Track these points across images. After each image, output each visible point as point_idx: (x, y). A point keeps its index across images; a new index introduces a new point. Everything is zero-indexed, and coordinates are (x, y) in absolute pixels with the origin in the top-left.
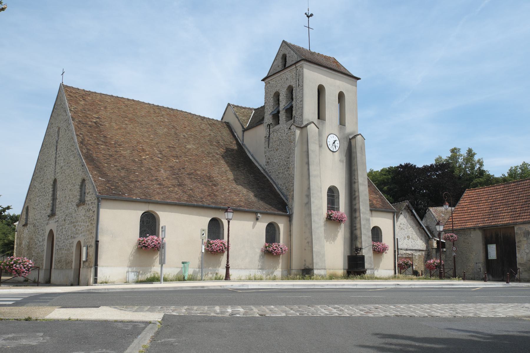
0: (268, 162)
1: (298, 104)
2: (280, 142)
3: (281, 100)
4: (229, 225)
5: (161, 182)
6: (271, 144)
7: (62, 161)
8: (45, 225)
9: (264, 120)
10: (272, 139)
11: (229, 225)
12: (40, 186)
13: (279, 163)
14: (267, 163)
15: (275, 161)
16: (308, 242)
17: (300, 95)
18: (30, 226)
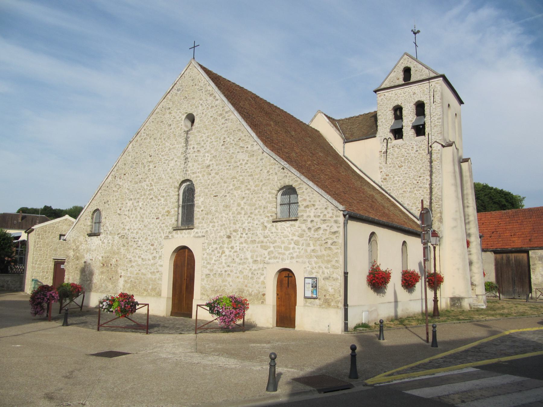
15: (398, 179)
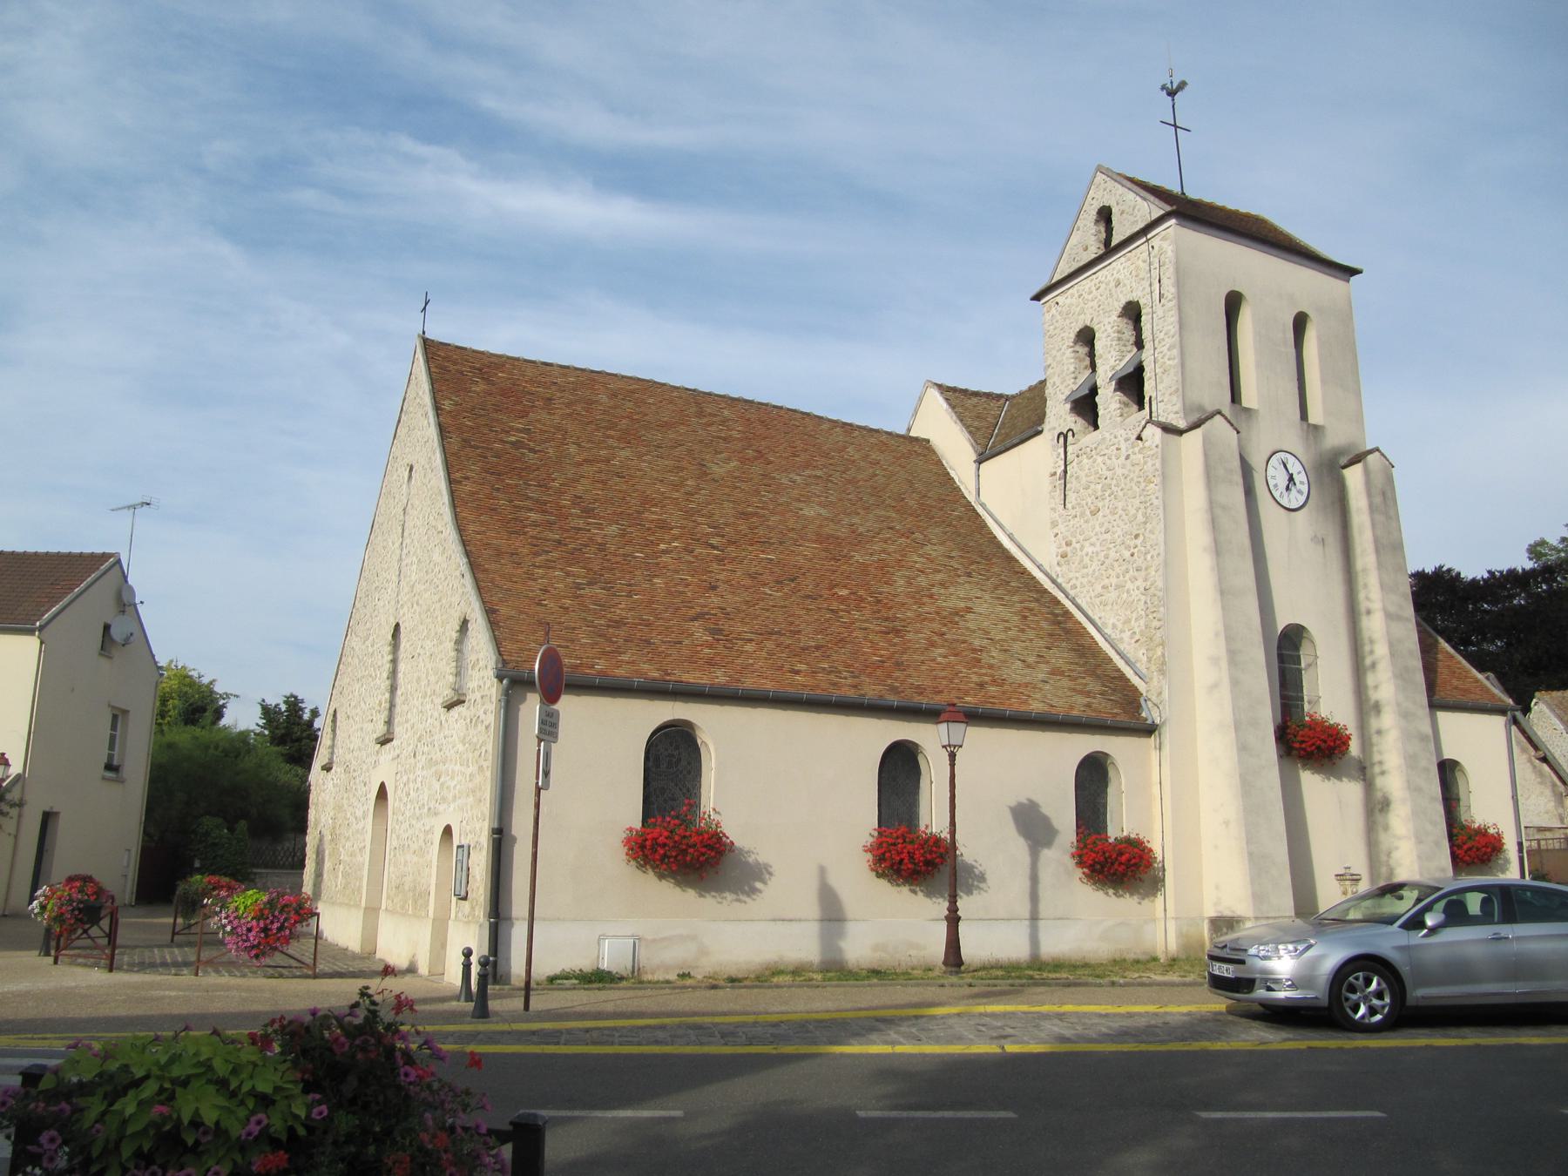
0: (1064, 556)
1: (1162, 358)
2: (1102, 487)
3: (1101, 352)
4: (952, 765)
5: (718, 625)
6: (1071, 496)
7: (415, 567)
8: (371, 768)
9: (1047, 420)
10: (1077, 478)
11: (952, 765)
12: (363, 647)
13: (1103, 554)
14: (1062, 557)
15: (1090, 549)
16: (1224, 822)
17: (1166, 328)
18: (339, 770)
